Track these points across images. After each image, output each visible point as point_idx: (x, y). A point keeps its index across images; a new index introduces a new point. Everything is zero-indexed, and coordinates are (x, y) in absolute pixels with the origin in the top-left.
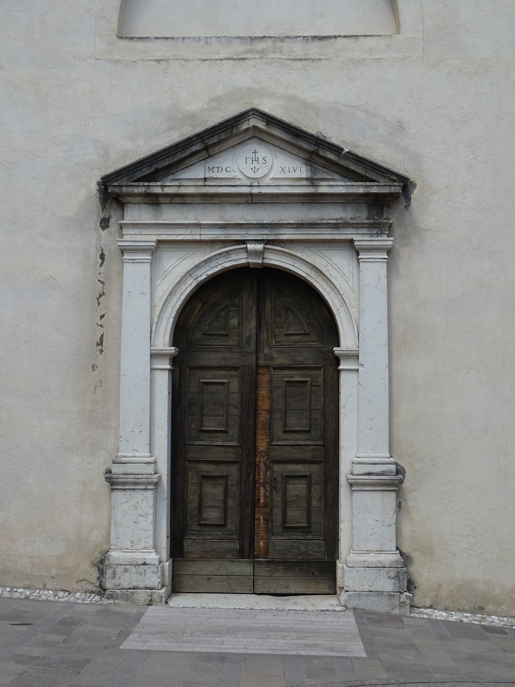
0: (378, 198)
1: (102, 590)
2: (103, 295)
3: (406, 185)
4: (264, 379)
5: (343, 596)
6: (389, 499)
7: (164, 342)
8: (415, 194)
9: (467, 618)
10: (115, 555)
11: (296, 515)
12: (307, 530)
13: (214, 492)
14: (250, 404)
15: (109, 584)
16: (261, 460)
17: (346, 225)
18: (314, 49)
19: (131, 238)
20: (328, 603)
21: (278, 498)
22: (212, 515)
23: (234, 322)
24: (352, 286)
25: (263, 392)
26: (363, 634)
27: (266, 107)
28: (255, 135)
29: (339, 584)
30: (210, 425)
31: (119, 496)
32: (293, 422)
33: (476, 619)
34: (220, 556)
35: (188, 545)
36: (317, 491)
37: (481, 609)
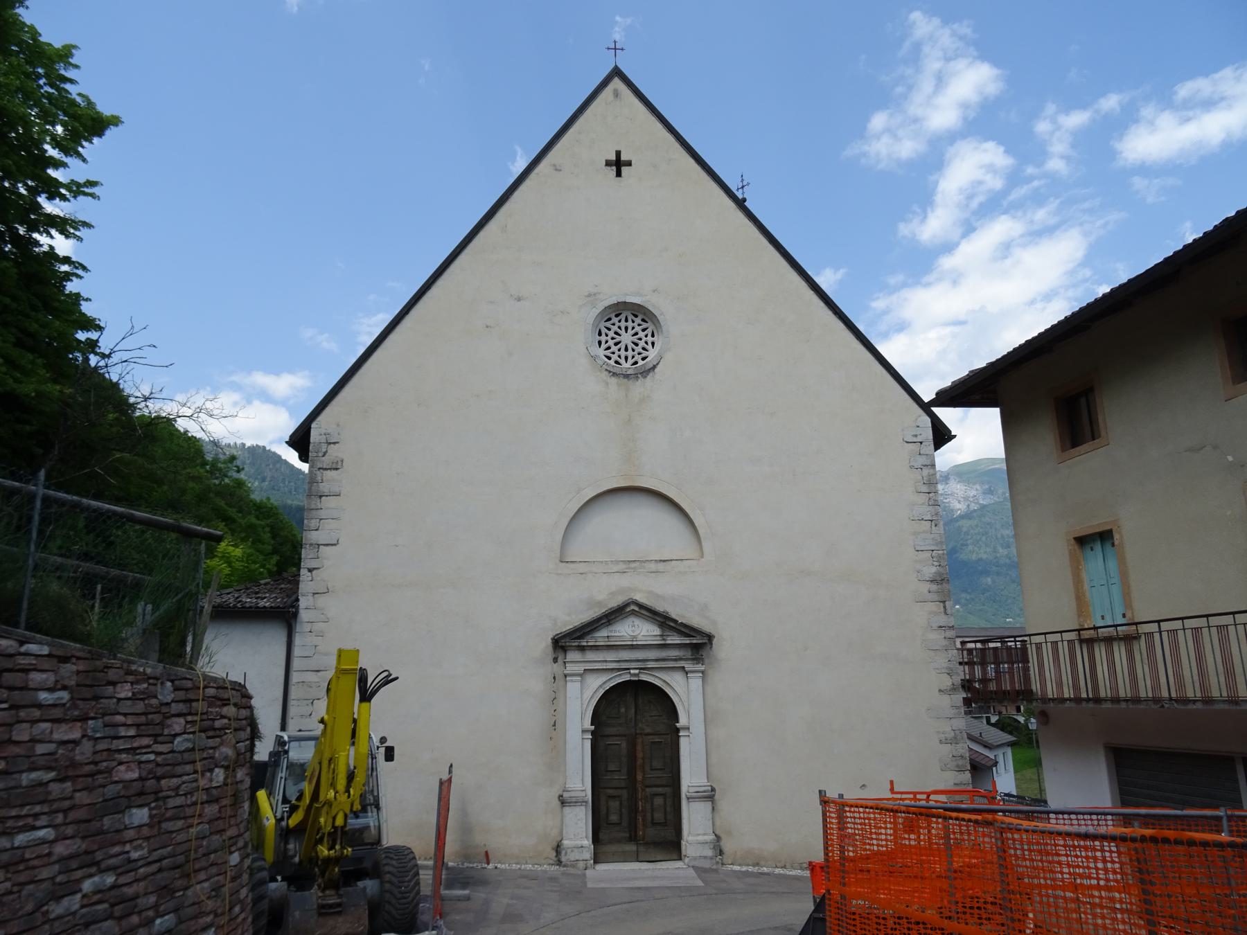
0: (696, 645)
1: (559, 863)
2: (555, 699)
3: (710, 637)
4: (639, 741)
5: (687, 860)
6: (279, 636)
7: (588, 724)
8: (715, 641)
9: (750, 869)
10: (566, 843)
11: (659, 816)
12: (665, 824)
13: (614, 804)
14: (632, 755)
15: (563, 859)
16: (639, 786)
17: (681, 659)
18: (661, 567)
19: (570, 668)
20: (679, 864)
21: (648, 807)
22: (614, 818)
23: (623, 710)
24: (684, 690)
25: (639, 748)
26: (700, 877)
27: (640, 598)
28: (633, 613)
29: (683, 853)
30: (612, 767)
31: (567, 810)
32: (656, 764)
33: (755, 869)
34: (619, 841)
35: (602, 836)
36: (669, 802)
37: (758, 864)
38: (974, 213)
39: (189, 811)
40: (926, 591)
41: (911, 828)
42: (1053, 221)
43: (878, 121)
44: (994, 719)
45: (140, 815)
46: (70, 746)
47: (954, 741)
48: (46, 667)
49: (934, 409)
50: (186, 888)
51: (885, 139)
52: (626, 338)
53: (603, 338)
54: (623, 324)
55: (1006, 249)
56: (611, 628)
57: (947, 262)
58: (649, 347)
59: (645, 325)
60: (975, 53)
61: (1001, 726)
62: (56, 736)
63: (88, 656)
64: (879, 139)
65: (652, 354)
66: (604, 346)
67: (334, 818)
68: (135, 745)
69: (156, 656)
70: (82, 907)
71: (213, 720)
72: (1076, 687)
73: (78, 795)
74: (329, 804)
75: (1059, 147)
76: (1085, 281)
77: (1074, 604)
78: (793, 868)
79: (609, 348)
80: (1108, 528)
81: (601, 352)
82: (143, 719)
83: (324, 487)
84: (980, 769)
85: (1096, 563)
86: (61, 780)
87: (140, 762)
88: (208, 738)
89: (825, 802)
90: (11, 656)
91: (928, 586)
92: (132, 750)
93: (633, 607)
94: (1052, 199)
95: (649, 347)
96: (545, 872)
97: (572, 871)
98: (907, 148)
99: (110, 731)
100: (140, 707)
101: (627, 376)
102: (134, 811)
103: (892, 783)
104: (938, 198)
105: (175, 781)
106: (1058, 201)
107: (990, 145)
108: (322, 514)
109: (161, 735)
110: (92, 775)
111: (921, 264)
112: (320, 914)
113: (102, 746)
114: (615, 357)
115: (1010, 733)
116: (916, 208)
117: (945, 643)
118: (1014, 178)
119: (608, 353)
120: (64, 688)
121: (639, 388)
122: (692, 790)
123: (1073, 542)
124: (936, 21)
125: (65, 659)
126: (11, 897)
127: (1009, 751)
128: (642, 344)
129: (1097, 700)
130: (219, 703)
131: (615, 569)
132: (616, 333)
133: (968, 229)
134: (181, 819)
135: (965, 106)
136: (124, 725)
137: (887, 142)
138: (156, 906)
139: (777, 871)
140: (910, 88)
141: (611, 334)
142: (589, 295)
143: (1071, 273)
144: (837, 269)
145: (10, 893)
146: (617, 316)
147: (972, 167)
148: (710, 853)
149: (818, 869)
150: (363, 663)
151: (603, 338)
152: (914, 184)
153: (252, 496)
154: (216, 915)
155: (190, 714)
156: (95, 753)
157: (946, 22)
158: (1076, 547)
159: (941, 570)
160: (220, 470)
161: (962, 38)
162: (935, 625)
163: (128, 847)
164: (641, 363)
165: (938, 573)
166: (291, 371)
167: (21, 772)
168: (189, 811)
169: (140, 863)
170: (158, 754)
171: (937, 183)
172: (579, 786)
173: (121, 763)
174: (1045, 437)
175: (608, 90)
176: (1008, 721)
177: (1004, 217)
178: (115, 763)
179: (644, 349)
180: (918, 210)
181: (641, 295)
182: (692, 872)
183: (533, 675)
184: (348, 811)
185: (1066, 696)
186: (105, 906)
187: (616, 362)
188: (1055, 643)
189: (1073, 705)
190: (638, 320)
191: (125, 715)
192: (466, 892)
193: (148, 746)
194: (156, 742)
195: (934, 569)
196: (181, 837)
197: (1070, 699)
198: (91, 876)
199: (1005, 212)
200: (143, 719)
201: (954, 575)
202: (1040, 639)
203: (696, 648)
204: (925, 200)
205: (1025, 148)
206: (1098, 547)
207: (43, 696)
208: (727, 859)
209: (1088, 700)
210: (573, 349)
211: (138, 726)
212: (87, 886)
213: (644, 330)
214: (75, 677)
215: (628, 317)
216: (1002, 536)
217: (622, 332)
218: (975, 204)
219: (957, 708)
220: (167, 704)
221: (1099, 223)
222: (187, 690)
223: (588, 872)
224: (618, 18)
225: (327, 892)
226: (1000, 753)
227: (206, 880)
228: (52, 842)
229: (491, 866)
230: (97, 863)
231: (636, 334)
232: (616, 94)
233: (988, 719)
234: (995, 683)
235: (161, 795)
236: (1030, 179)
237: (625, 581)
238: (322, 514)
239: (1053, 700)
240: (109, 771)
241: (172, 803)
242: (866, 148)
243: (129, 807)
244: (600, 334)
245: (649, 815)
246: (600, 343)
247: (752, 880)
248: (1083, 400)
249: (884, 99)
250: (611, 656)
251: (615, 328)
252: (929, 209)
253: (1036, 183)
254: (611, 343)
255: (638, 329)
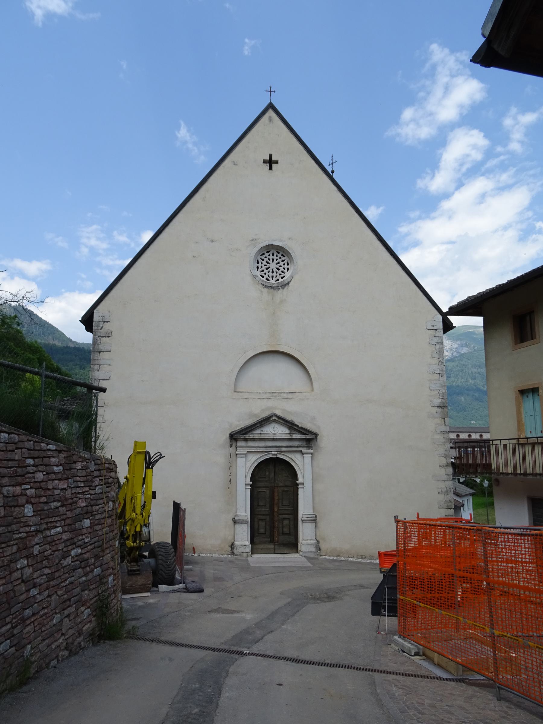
0: (308, 439)
1: (233, 553)
2: (231, 467)
3: (316, 435)
4: (276, 490)
5: (301, 553)
7: (248, 481)
8: (319, 437)
9: (335, 558)
10: (237, 543)
11: (286, 530)
12: (289, 534)
13: (262, 524)
15: (235, 552)
16: (276, 514)
17: (300, 447)
18: (290, 396)
19: (239, 450)
20: (297, 555)
21: (281, 525)
22: (262, 531)
23: (267, 473)
24: (302, 464)
25: (276, 494)
28: (275, 421)
29: (299, 549)
31: (237, 526)
33: (338, 558)
34: (265, 543)
35: (255, 540)
36: (292, 523)
37: (339, 556)
38: (464, 175)
39: (103, 521)
40: (435, 412)
41: (426, 536)
42: (511, 181)
43: (408, 114)
44: (462, 480)
45: (87, 523)
46: (64, 491)
47: (446, 493)
48: (55, 455)
49: (448, 317)
50: (103, 556)
51: (412, 126)
52: (273, 266)
53: (260, 265)
54: (271, 257)
55: (482, 197)
56: (262, 429)
57: (446, 205)
58: (286, 271)
59: (283, 258)
60: (470, 73)
61: (466, 484)
62: (60, 487)
63: (66, 450)
64: (407, 125)
65: (287, 275)
66: (260, 270)
67: (136, 527)
68: (84, 491)
69: (82, 448)
70: (72, 562)
71: (108, 479)
72: (515, 467)
73: (68, 513)
74: (133, 520)
75: (517, 135)
76: (529, 219)
77: (516, 425)
78: (357, 558)
79: (263, 271)
80: (537, 386)
81: (258, 273)
82: (85, 479)
83: (102, 347)
84: (458, 508)
85: (529, 403)
86: (62, 506)
87: (86, 498)
88: (107, 487)
89: (397, 521)
90: (45, 451)
91: (436, 409)
92: (82, 493)
93: (274, 418)
94: (511, 168)
95: (286, 271)
96: (226, 558)
97: (239, 557)
98: (425, 132)
99: (75, 484)
100: (84, 473)
101: (273, 288)
102: (85, 520)
103: (418, 514)
104: (442, 164)
105: (97, 507)
106: (515, 169)
107: (475, 132)
108: (101, 362)
109: (92, 486)
110: (71, 504)
111: (430, 205)
112: (129, 575)
113: (74, 491)
114: (266, 276)
115: (472, 488)
116: (428, 170)
117: (444, 440)
118: (489, 154)
119: (262, 274)
120: (61, 465)
121: (280, 294)
122: (305, 516)
123: (518, 392)
124: (447, 51)
125: (60, 452)
126: (52, 556)
127: (471, 498)
128: (281, 269)
129: (525, 474)
130: (109, 471)
131: (265, 396)
132: (267, 262)
133: (460, 185)
134: (100, 525)
135: (461, 106)
136: (80, 481)
137: (413, 128)
138: (94, 564)
139: (349, 559)
140: (428, 93)
141: (264, 263)
142: (252, 240)
143: (521, 213)
144: (378, 207)
145: (51, 555)
146: (268, 252)
147: (465, 145)
148: (313, 549)
149: (383, 555)
150: (147, 449)
151: (260, 265)
152: (428, 155)
153: (26, 340)
154: (113, 569)
155: (100, 476)
156: (72, 494)
157: (453, 51)
158: (519, 395)
159: (444, 401)
160: (8, 324)
161: (462, 63)
162: (439, 431)
163: (84, 537)
164: (281, 280)
165: (442, 403)
166: (39, 260)
167: (51, 502)
168: (103, 521)
169: (88, 544)
170: (91, 495)
171: (441, 155)
172: (244, 513)
173: (80, 499)
174: (506, 336)
175: (266, 117)
176: (470, 481)
177: (482, 178)
178: (78, 499)
179: (283, 272)
180: (429, 172)
181: (282, 241)
182: (304, 559)
183: (219, 454)
184: (143, 523)
185: (510, 472)
186: (78, 562)
187: (267, 279)
188: (505, 445)
189: (513, 476)
190: (280, 255)
191: (80, 477)
192: (190, 567)
193: (88, 491)
194: (90, 489)
195: (439, 401)
196: (100, 533)
197: (511, 474)
198: (74, 549)
199: (483, 175)
200: (85, 479)
201: (449, 402)
202: (498, 442)
203: (309, 441)
204: (434, 166)
205: (496, 134)
206: (531, 395)
207: (55, 468)
208: (322, 553)
209: (520, 474)
210: (242, 271)
211: (84, 481)
212: (73, 553)
213: (283, 261)
214: (64, 460)
215: (274, 255)
216: (472, 373)
217: (271, 262)
218: (464, 169)
219: (448, 475)
220: (93, 471)
221: (539, 183)
222: (99, 465)
223: (248, 558)
224: (247, 40)
225: (132, 564)
226: (465, 499)
227: (109, 553)
228: (61, 533)
229: (196, 555)
230: (75, 544)
231: (278, 263)
232: (270, 120)
233: (459, 480)
234: (471, 464)
235: (93, 513)
236: (499, 155)
237: (270, 403)
238: (101, 362)
239: (503, 473)
240: (76, 503)
241: (98, 517)
242: (399, 131)
243: (83, 519)
244: (258, 263)
245: (281, 529)
246: (258, 268)
247: (337, 564)
248: (528, 318)
249: (411, 99)
250: (262, 444)
251: (266, 259)
252: (436, 172)
253: (502, 157)
254: (264, 268)
255: (279, 260)
